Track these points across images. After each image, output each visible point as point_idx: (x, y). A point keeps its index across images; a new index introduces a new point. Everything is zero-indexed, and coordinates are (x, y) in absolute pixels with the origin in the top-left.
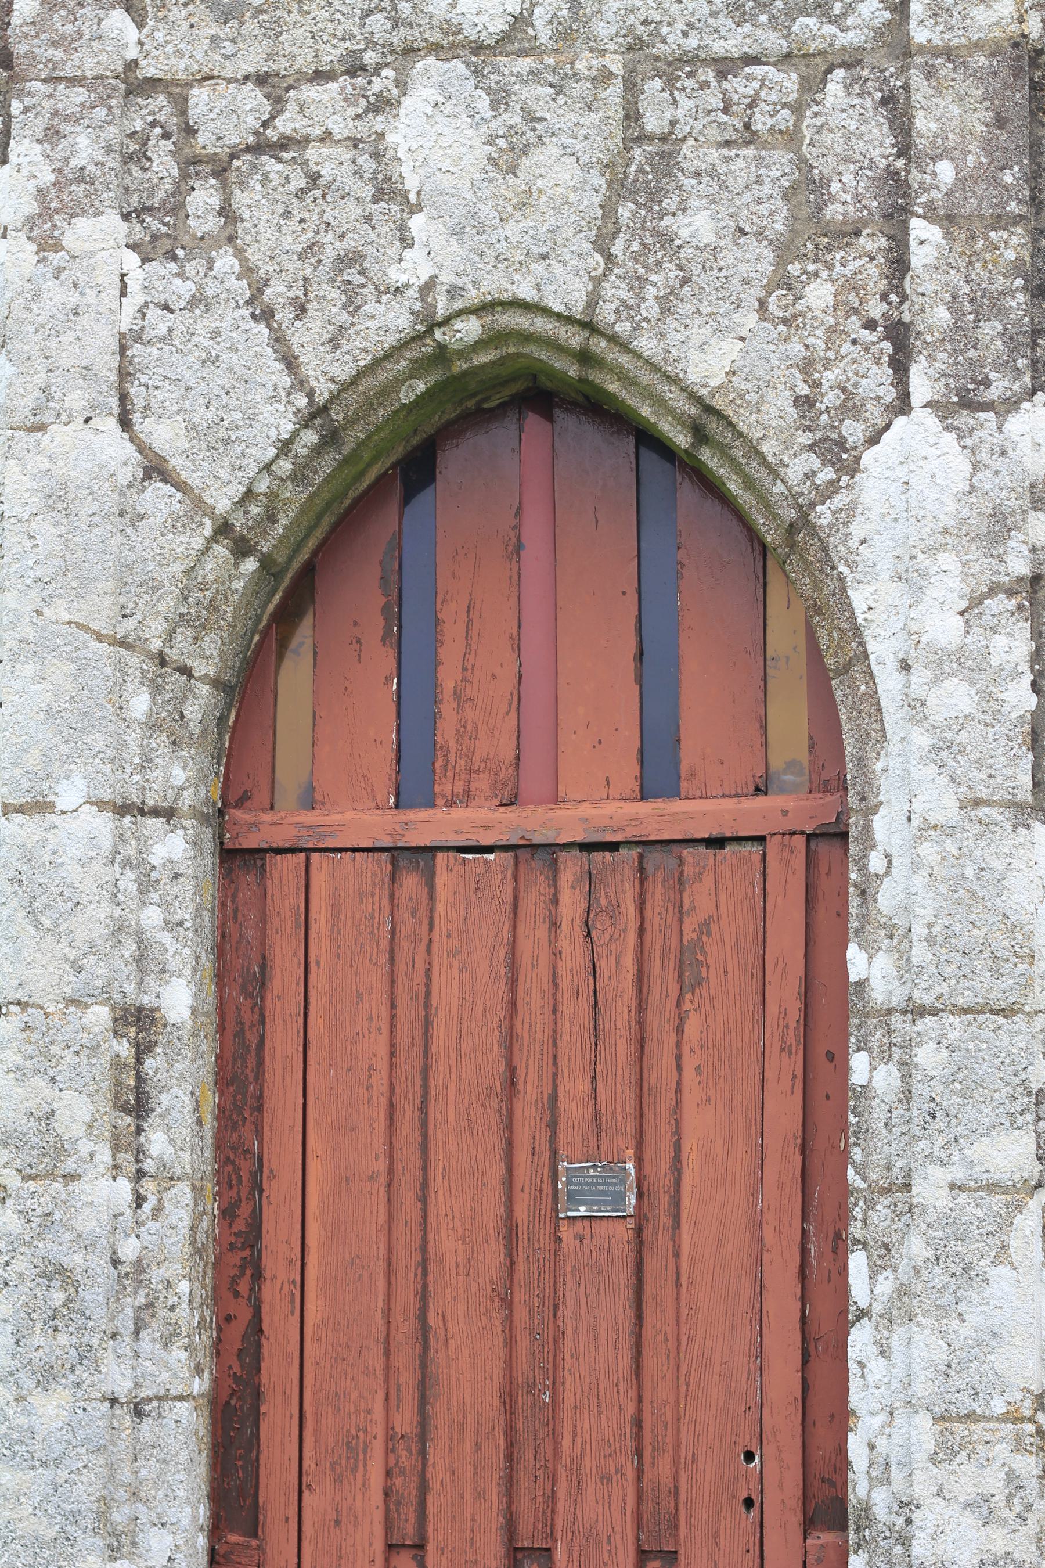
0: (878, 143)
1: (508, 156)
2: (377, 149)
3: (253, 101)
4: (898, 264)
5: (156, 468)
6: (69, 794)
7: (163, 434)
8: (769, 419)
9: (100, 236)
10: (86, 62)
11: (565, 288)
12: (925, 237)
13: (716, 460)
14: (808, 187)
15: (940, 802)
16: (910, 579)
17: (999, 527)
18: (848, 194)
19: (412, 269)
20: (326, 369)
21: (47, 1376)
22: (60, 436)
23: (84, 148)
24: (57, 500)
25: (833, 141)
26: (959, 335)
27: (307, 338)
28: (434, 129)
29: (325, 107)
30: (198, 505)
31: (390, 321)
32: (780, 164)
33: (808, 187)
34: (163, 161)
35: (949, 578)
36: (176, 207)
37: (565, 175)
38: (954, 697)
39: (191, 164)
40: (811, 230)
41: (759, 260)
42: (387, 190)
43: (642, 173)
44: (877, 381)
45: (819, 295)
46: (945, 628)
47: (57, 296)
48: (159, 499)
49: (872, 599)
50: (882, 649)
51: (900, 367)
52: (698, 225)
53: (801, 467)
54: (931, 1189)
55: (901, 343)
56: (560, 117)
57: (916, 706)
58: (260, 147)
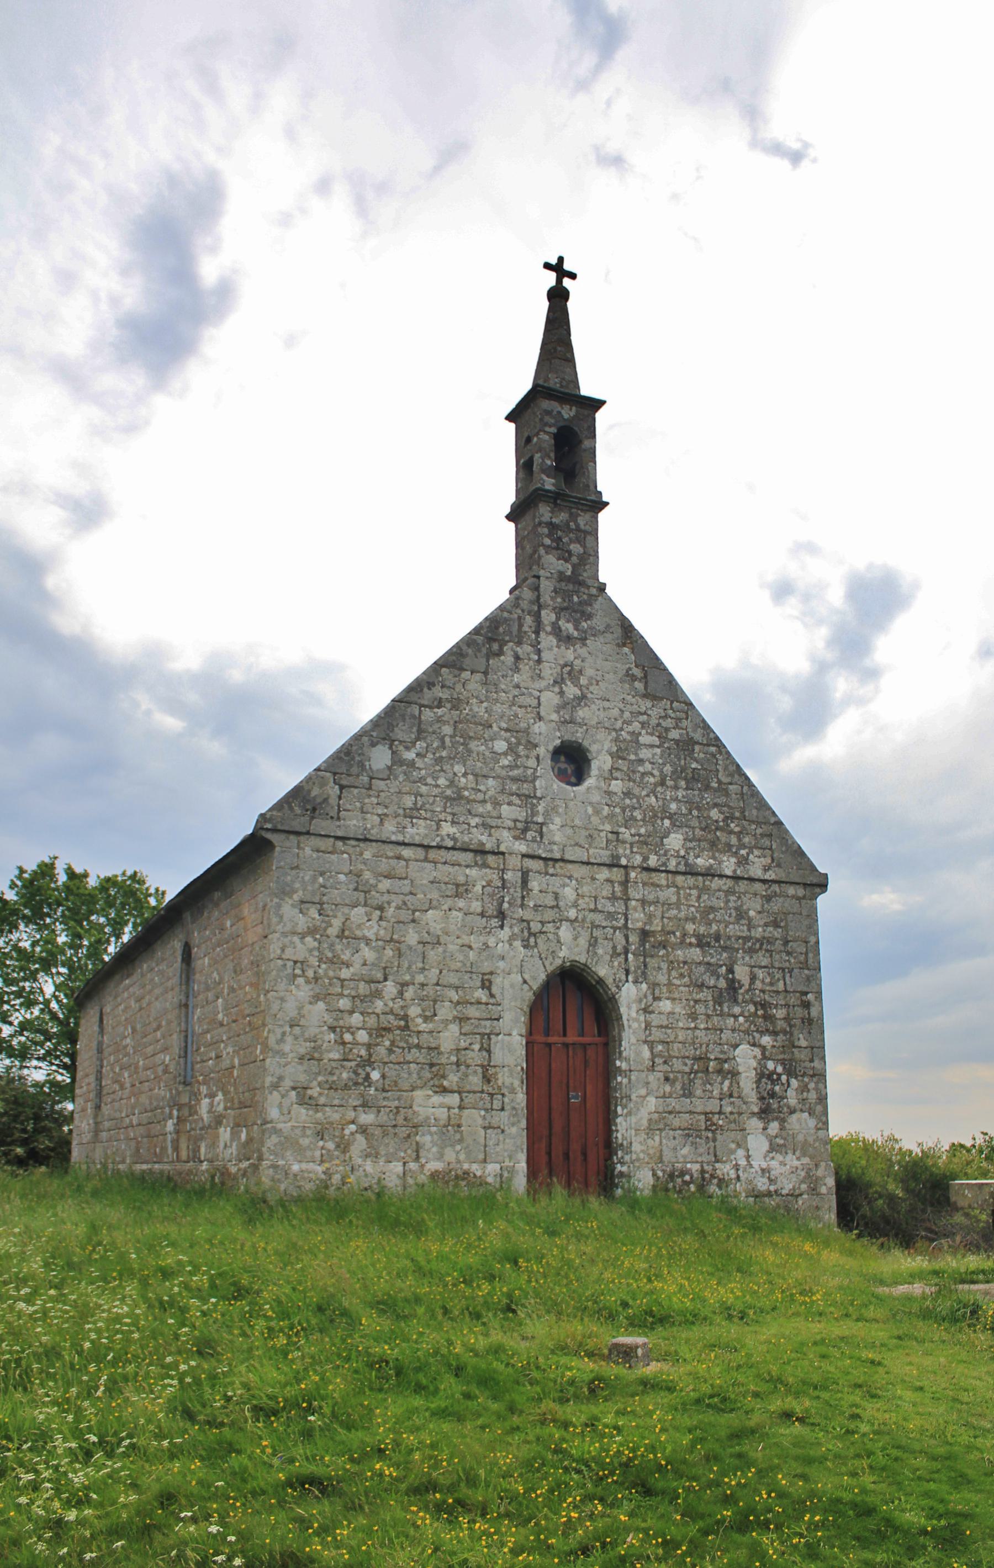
0: (624, 942)
1: (575, 939)
2: (557, 934)
3: (539, 925)
4: (626, 959)
5: (525, 982)
6: (514, 1033)
7: (526, 977)
8: (609, 981)
9: (518, 944)
10: (516, 916)
11: (583, 960)
12: (630, 956)
13: (83, 1479)
14: (614, 948)
15: (633, 1040)
16: (629, 1008)
17: (640, 1001)
18: (619, 949)
19: (562, 954)
20: (550, 969)
21: (513, 1125)
22: (513, 976)
23: (516, 930)
24: (512, 986)
25: (246, 1386)
26: (635, 972)
27: (547, 963)
28: (565, 932)
29: (549, 927)
30: (531, 988)
31: (558, 962)
32: (611, 944)
33: (614, 948)
34: (526, 934)
35: (634, 1007)
36: (528, 940)
37: (583, 942)
38: (635, 1025)
39: (530, 934)
40: (615, 954)
41: (608, 957)
42: (559, 941)
43: (593, 943)
44: (624, 977)
45: (616, 964)
46: (634, 1015)
47: (512, 953)
48: (525, 986)
49: (623, 1010)
50: (625, 1017)
51: (627, 975)
52: (600, 951)
53: (614, 989)
54: (633, 1097)
55: (627, 972)
56: (583, 933)
57: (630, 1027)
58: (541, 932)
